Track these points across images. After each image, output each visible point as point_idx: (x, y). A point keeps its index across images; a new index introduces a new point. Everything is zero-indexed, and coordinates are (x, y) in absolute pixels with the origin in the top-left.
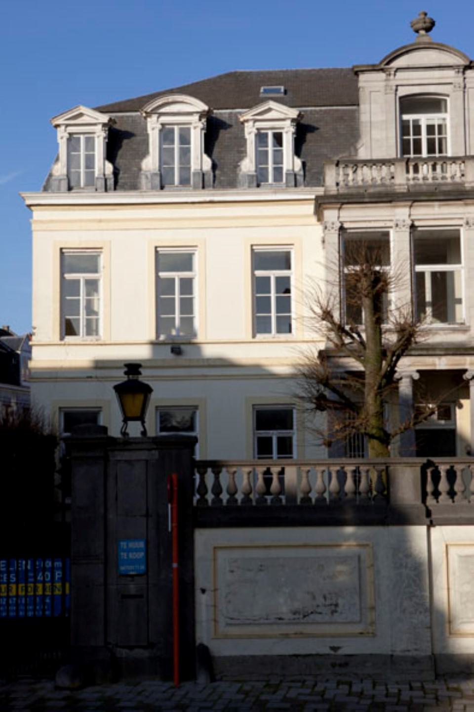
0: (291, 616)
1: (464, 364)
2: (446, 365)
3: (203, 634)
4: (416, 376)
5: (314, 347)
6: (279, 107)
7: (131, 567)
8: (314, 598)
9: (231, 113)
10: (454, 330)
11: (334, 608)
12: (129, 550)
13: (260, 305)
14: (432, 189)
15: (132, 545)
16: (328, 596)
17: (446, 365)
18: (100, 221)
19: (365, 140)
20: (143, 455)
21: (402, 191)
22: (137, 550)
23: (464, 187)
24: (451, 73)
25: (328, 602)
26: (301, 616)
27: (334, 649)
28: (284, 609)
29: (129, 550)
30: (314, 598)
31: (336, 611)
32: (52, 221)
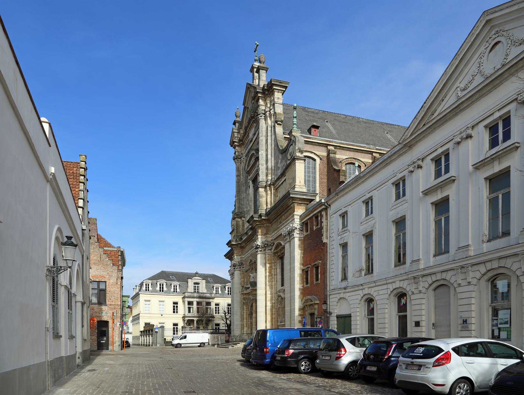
13: (174, 309)
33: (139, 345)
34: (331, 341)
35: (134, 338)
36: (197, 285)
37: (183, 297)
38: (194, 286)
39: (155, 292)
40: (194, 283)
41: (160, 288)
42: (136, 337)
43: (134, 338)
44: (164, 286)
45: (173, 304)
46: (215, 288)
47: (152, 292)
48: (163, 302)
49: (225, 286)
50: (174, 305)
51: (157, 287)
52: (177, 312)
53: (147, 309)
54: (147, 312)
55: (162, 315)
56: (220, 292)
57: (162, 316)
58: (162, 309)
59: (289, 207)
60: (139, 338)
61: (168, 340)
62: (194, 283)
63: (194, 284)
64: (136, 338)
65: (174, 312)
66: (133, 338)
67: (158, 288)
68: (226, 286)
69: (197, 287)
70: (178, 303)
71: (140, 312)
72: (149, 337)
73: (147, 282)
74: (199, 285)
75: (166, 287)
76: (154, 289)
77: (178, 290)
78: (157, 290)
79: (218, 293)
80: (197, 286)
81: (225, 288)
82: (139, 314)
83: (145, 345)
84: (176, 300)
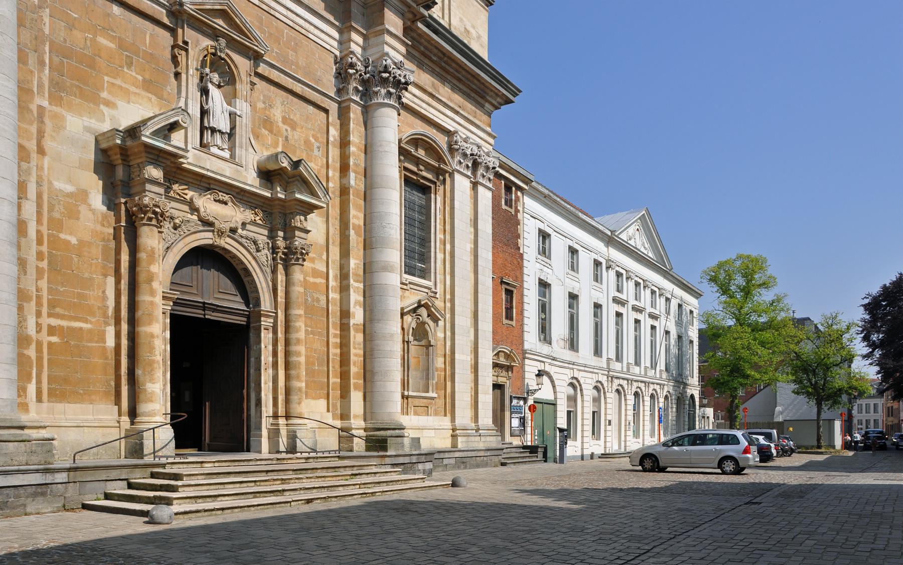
59: (483, 97)
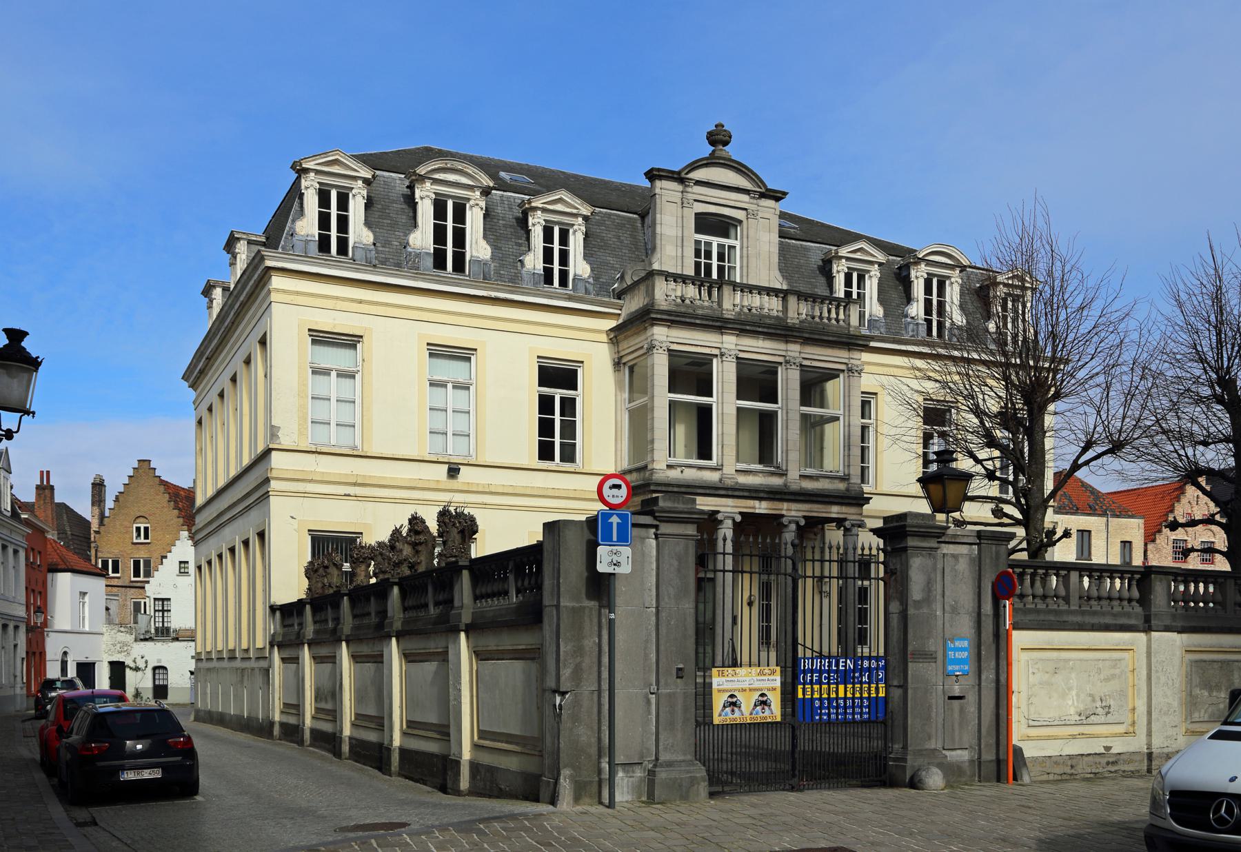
0: (1078, 718)
1: (782, 510)
2: (766, 509)
3: (1019, 733)
4: (738, 518)
5: (1133, 448)
6: (572, 200)
7: (957, 667)
8: (1094, 701)
9: (502, 196)
10: (772, 474)
11: (1108, 710)
12: (956, 649)
13: (546, 428)
14: (756, 319)
15: (957, 644)
16: (1104, 698)
17: (766, 509)
18: (361, 302)
19: (657, 255)
20: (964, 549)
21: (730, 317)
22: (962, 649)
23: (787, 323)
24: (745, 198)
25: (1104, 704)
26: (1084, 718)
27: (1108, 748)
28: (1072, 711)
29: (956, 649)
30: (1094, 701)
31: (1109, 713)
32: (298, 293)
33: (262, 729)
34: (668, 781)
35: (215, 664)
36: (715, 241)
37: (612, 323)
38: (698, 242)
39: (398, 265)
40: (698, 216)
41: (324, 221)
42: (232, 658)
43: (215, 664)
44: (571, 248)
45: (540, 385)
46: (536, 224)
47: (373, 266)
48: (350, 342)
49: (525, 214)
50: (547, 390)
51: (415, 225)
52: (569, 454)
53: (334, 412)
54: (334, 438)
55: (453, 471)
56: (579, 267)
57: (453, 484)
58: (454, 423)
60: (266, 672)
61: (733, 704)
62: (698, 216)
63: (698, 230)
64: (225, 664)
65: (546, 452)
66: (204, 665)
67: (422, 239)
68: (422, 179)
69: (721, 257)
70: (574, 373)
71: (273, 432)
72: (327, 660)
73: (335, 169)
74: (727, 236)
75: (368, 224)
76: (387, 243)
77: (579, 267)
78: (418, 255)
79: (564, 275)
80: (721, 246)
81: (528, 232)
82: (267, 452)
83: (346, 748)
84: (561, 350)
